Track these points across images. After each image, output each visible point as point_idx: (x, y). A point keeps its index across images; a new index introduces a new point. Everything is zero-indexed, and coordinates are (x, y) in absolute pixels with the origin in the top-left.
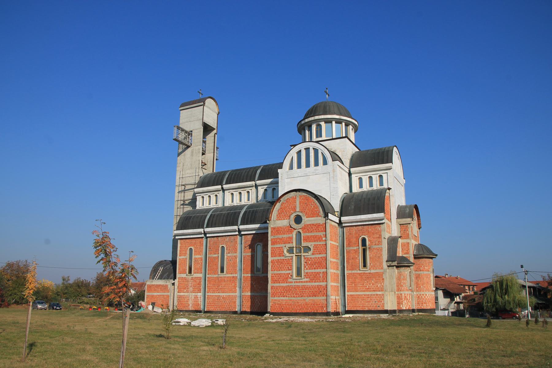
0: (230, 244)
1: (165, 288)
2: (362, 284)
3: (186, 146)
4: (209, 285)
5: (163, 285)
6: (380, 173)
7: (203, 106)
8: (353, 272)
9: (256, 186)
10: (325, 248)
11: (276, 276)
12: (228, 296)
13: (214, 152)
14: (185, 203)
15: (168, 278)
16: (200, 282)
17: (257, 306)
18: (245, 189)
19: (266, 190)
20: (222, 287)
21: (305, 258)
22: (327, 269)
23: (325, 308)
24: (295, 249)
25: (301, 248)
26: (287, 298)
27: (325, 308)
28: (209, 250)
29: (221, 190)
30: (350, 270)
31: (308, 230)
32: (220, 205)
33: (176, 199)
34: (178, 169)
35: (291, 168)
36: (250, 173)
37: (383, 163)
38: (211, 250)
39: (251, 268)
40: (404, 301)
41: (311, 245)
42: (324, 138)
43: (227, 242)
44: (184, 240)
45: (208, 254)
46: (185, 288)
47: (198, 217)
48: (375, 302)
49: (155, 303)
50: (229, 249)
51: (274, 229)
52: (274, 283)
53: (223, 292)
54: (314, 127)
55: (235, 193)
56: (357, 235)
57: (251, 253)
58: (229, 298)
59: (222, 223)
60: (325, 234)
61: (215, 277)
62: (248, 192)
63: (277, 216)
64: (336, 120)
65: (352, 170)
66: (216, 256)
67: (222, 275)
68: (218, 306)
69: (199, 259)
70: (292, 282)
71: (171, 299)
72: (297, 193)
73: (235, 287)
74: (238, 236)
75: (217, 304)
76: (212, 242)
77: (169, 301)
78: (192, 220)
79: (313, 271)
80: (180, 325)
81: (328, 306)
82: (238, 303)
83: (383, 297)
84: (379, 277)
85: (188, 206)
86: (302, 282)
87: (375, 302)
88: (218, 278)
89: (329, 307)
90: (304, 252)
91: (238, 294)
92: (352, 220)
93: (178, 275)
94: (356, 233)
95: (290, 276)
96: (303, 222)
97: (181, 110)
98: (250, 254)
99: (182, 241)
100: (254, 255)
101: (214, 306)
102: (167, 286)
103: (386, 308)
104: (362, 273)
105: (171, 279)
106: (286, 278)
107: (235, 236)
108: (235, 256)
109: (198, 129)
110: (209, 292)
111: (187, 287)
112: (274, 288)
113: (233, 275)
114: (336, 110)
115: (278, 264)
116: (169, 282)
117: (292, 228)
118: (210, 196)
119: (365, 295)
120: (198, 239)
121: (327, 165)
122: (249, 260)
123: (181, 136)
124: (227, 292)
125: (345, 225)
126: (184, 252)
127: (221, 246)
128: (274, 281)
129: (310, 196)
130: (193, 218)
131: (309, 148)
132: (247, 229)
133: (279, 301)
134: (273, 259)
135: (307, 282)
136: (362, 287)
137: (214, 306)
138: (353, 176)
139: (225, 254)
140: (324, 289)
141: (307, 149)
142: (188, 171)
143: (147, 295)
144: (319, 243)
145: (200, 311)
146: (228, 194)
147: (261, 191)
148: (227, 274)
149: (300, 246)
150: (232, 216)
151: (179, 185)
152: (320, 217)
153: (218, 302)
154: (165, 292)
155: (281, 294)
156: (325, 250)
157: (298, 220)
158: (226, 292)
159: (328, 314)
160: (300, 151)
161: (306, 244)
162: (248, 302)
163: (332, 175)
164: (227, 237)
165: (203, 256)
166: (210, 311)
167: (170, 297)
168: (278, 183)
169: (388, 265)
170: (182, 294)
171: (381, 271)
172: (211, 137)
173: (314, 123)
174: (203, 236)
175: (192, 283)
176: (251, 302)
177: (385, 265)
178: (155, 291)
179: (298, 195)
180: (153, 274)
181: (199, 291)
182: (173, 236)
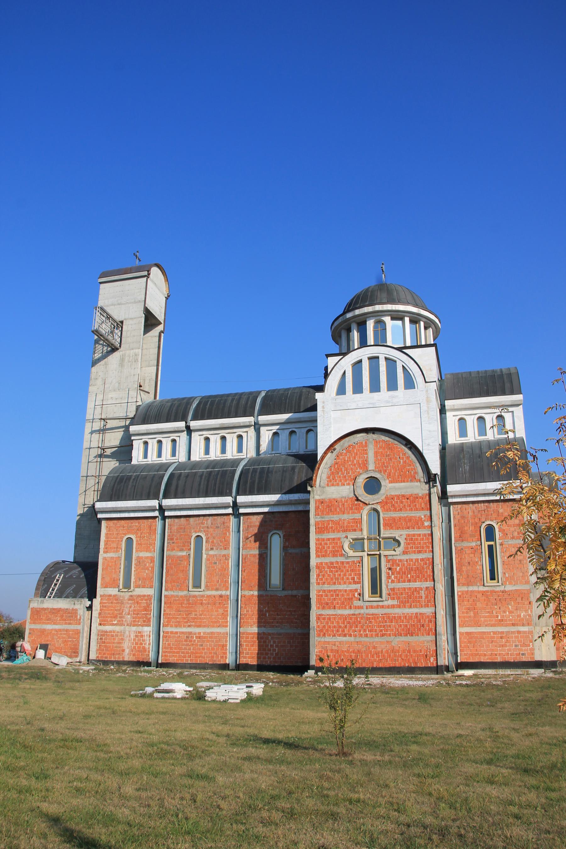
0: (214, 531)
1: (71, 615)
2: (489, 612)
3: (109, 349)
4: (168, 611)
5: (67, 609)
6: (480, 413)
7: (145, 278)
8: (471, 588)
9: (257, 427)
10: (430, 541)
11: (327, 596)
12: (208, 633)
13: (158, 365)
14: (105, 454)
15: (75, 595)
16: (148, 605)
18: (234, 430)
19: (275, 434)
20: (196, 615)
21: (388, 561)
22: (434, 580)
23: (432, 659)
24: (366, 541)
25: (379, 542)
26: (352, 639)
27: (432, 659)
28: (168, 543)
29: (183, 431)
30: (464, 585)
31: (393, 506)
32: (182, 457)
33: (86, 445)
34: (91, 389)
35: (341, 390)
36: (243, 402)
37: (504, 393)
38: (173, 543)
39: (259, 579)
41: (401, 535)
43: (208, 527)
44: (115, 522)
45: (167, 551)
46: (115, 617)
47: (146, 477)
48: (516, 646)
49: (47, 645)
50: (213, 542)
51: (322, 503)
52: (323, 608)
53: (199, 626)
54: (370, 324)
55: (212, 438)
57: (258, 550)
58: (211, 637)
59: (199, 492)
60: (429, 514)
61: (182, 596)
62: (240, 437)
63: (329, 477)
64: (412, 315)
66: (184, 553)
67: (196, 592)
68: (187, 653)
69: (146, 560)
70: (362, 607)
71: (83, 637)
72: (368, 435)
73: (225, 616)
74: (232, 517)
75: (185, 649)
76: (175, 527)
77: (79, 642)
78: (133, 482)
79: (406, 585)
80: (175, 698)
81: (440, 654)
85: (111, 459)
86: (383, 607)
87: (516, 646)
88: (187, 598)
89: (441, 656)
90: (386, 549)
91: (230, 629)
92: (468, 491)
93: (100, 591)
94: (474, 516)
95: (356, 596)
96: (383, 491)
97: (101, 283)
98: (257, 552)
99: (111, 523)
100: (266, 553)
101: (178, 653)
102: (75, 612)
103: (537, 658)
104: (487, 591)
105: (82, 597)
107: (225, 517)
108: (224, 556)
109: (135, 318)
110: (167, 626)
111: (120, 614)
112: (324, 619)
113: (219, 593)
114: (409, 298)
115: (331, 571)
116: (81, 604)
117: (361, 501)
118: (160, 442)
119: (494, 633)
120: (145, 521)
121: (415, 388)
122: (255, 563)
124: (208, 626)
125: (454, 501)
126: (114, 545)
127: (194, 535)
128: (323, 605)
129: (396, 442)
130: (134, 479)
131: (378, 358)
132: (254, 504)
133: (335, 645)
134: (319, 560)
135: (393, 606)
136: (489, 617)
137: (178, 653)
138: (449, 414)
139: (204, 551)
140: (431, 621)
141: (374, 359)
143: (30, 629)
144: (416, 532)
145: (147, 662)
146: (198, 440)
147: (266, 435)
148: (208, 590)
149: (378, 537)
150: (219, 477)
151: (93, 419)
152: (417, 482)
153: (188, 645)
154: (70, 624)
155: (338, 631)
156: (431, 545)
158: (204, 626)
159: (438, 670)
160: (360, 361)
161: (391, 534)
162: (252, 646)
163: (424, 408)
164: (208, 517)
165: (156, 554)
166: (170, 663)
167: (81, 635)
168: (316, 421)
170: (108, 628)
172: (152, 337)
173: (371, 318)
174: (156, 514)
175: (131, 607)
176: (260, 646)
178: (49, 621)
179: (371, 440)
181: (147, 623)
182: (78, 516)
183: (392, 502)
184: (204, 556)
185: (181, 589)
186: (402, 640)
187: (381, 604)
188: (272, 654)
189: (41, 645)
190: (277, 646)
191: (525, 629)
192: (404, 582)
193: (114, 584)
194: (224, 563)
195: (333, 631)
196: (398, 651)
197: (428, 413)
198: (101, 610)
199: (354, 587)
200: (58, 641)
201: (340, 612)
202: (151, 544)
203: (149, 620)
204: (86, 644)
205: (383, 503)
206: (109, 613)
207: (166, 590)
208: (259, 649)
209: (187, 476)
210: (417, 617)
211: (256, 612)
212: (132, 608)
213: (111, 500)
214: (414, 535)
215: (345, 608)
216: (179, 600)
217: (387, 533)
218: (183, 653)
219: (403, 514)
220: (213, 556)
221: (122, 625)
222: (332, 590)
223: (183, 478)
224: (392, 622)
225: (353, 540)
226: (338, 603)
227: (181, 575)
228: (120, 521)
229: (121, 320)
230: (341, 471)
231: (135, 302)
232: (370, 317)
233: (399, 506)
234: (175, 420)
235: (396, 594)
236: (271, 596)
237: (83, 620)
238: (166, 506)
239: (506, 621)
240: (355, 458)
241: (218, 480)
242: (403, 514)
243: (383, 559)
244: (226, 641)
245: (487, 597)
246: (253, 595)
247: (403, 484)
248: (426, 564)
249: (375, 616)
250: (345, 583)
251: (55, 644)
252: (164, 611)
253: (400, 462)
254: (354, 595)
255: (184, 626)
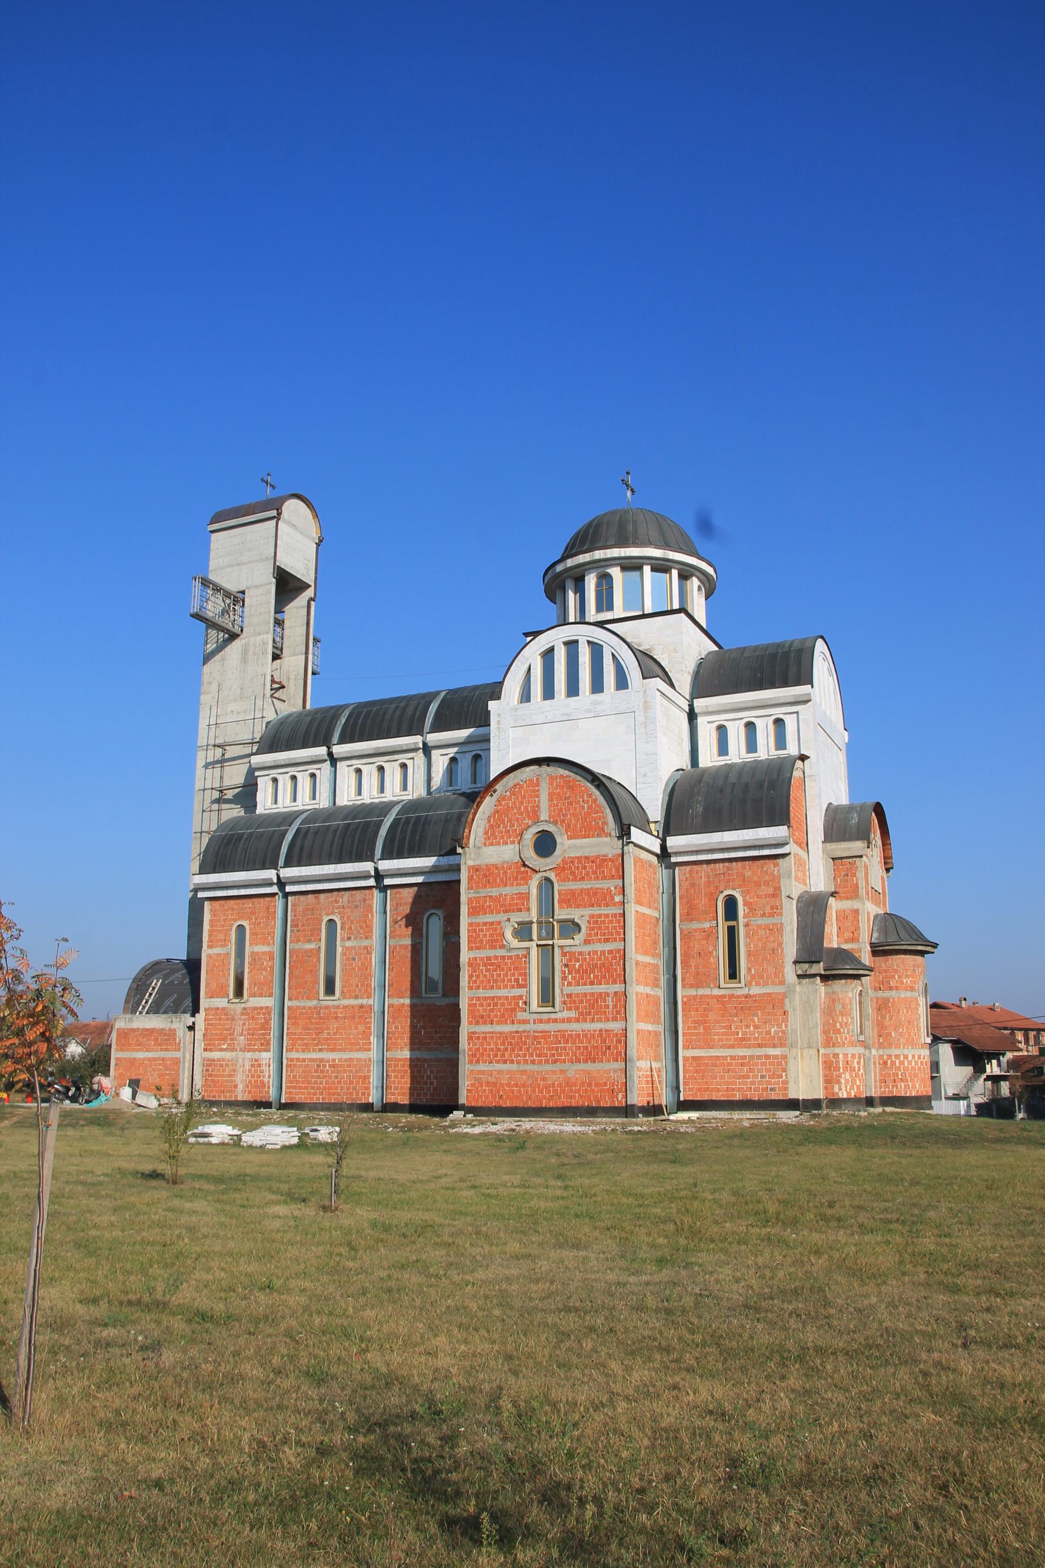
1: (167, 1038)
2: (726, 1027)
3: (226, 636)
4: (292, 1030)
5: (162, 1029)
7: (274, 522)
9: (427, 750)
11: (482, 1005)
12: (345, 1060)
13: (307, 653)
14: (225, 797)
15: (176, 1009)
16: (267, 1022)
17: (429, 1089)
18: (396, 757)
19: (453, 760)
20: (329, 1034)
21: (564, 954)
22: (625, 983)
23: (620, 1096)
24: (535, 926)
25: (553, 925)
26: (514, 1067)
27: (620, 1096)
29: (325, 761)
30: (692, 986)
31: (573, 873)
32: (323, 802)
33: (199, 785)
34: (204, 698)
35: (526, 696)
36: (410, 711)
38: (298, 931)
40: (843, 1076)
42: (618, 612)
43: (343, 907)
44: (222, 902)
46: (225, 1039)
47: (262, 834)
48: (762, 1077)
50: (350, 928)
51: (477, 870)
52: (477, 1023)
53: (333, 1050)
54: (591, 582)
56: (712, 889)
59: (330, 855)
61: (310, 1008)
63: (486, 833)
64: (654, 562)
65: (699, 704)
66: (312, 946)
67: (328, 1001)
69: (263, 957)
70: (527, 1022)
71: (184, 1068)
73: (367, 1035)
74: (375, 892)
75: (316, 1083)
76: (301, 908)
78: (244, 844)
79: (588, 989)
80: (210, 1144)
82: (374, 1080)
83: (786, 1063)
84: (775, 1005)
85: (233, 806)
86: (555, 1021)
87: (762, 1077)
88: (317, 1009)
89: (631, 1092)
91: (374, 1054)
92: (697, 845)
93: (204, 1003)
94: (709, 883)
97: (212, 532)
98: (408, 941)
99: (217, 904)
100: (421, 943)
101: (306, 1088)
102: (172, 1033)
103: (792, 1095)
104: (724, 996)
105: (184, 1012)
106: (510, 1010)
107: (367, 892)
108: (366, 948)
110: (291, 1050)
111: (231, 1034)
113: (359, 1002)
114: (654, 533)
115: (488, 970)
116: (180, 1021)
119: (733, 1058)
120: (261, 900)
121: (628, 688)
123: (214, 607)
127: (326, 919)
128: (477, 1019)
129: (579, 778)
130: (246, 839)
131: (577, 642)
133: (491, 1075)
134: (473, 954)
135: (569, 1020)
137: (306, 1088)
138: (701, 721)
140: (619, 1041)
141: (572, 645)
142: (233, 707)
143: (117, 1059)
144: (603, 911)
145: (266, 1102)
147: (440, 762)
148: (345, 998)
149: (551, 920)
151: (208, 745)
152: (606, 836)
153: (318, 1077)
154: (167, 1050)
155: (496, 1055)
156: (622, 931)
157: (545, 844)
158: (340, 1050)
160: (551, 650)
162: (403, 1077)
163: (640, 718)
164: (343, 893)
167: (181, 1065)
169: (800, 972)
170: (216, 1055)
171: (780, 989)
172: (297, 608)
174: (274, 889)
176: (413, 1078)
177: (790, 972)
180: (134, 1000)
183: (570, 867)
184: (339, 949)
185: (309, 998)
186: (580, 1068)
187: (553, 1016)
188: (429, 1089)
189: (130, 1080)
190: (435, 1077)
191: (777, 1052)
192: (585, 984)
193: (222, 993)
194: (366, 958)
195: (489, 1056)
196: (575, 1084)
197: (646, 726)
198: (206, 1029)
199: (517, 992)
200: (152, 1075)
201: (498, 1028)
202: (269, 934)
203: (268, 1044)
204: (188, 1078)
205: (558, 870)
206: (216, 1034)
207: (290, 999)
208: (412, 1083)
209: (317, 831)
210: (601, 1035)
211: (407, 1029)
212: (247, 1026)
213: (214, 872)
214: (600, 916)
215: (506, 1023)
216: (306, 1013)
217: (563, 913)
218: (313, 1088)
219: (586, 885)
220: (348, 948)
221: (233, 1050)
222: (488, 997)
223: (310, 836)
224: (567, 1043)
225: (519, 923)
226: (496, 1016)
227: (309, 978)
228: (228, 901)
229: (241, 589)
230: (504, 823)
231: (261, 560)
232: (589, 569)
233: (581, 873)
234: (315, 745)
235: (574, 1002)
236: (428, 1005)
237: (184, 1044)
238: (285, 878)
239: (749, 1039)
240: (522, 803)
241: (357, 835)
242: (586, 885)
243: (556, 950)
244: (369, 1071)
245: (723, 1004)
246: (403, 1005)
247: (586, 840)
248: (615, 958)
249: (545, 1034)
250: (506, 987)
251: (148, 1079)
252: (288, 1029)
253: (583, 807)
254: (517, 1004)
255: (314, 1050)
